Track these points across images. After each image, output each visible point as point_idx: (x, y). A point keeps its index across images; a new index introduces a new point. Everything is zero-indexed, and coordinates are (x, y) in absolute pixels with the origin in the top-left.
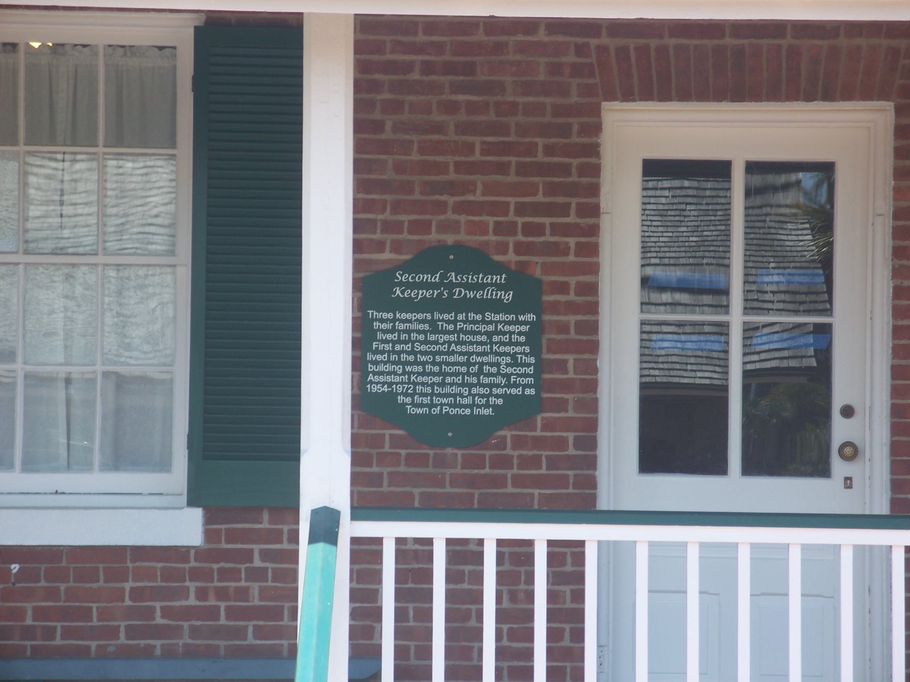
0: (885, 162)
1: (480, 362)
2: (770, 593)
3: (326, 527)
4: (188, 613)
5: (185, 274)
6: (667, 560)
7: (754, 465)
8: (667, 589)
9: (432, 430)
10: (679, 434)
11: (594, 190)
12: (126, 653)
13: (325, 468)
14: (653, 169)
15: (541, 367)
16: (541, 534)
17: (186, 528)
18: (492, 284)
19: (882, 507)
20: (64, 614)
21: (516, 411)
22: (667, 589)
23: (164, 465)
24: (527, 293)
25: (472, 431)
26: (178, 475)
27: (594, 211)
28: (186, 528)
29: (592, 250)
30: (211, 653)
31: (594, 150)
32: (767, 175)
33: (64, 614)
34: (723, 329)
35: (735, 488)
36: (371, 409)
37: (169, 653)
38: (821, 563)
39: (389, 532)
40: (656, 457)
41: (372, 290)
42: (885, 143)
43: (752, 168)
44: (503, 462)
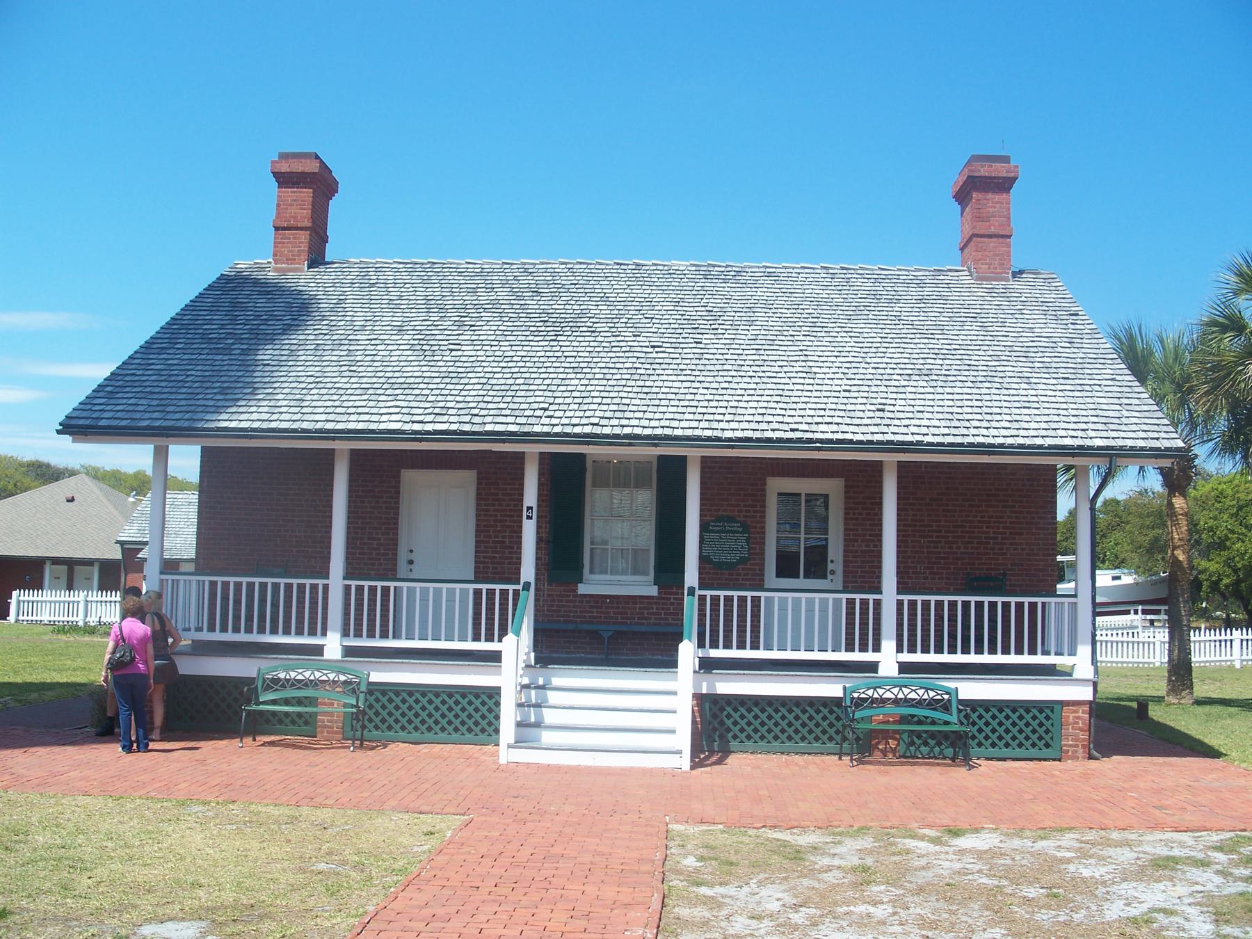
0: (842, 495)
1: (733, 547)
2: (810, 610)
3: (692, 592)
4: (654, 614)
5: (654, 522)
6: (783, 602)
7: (807, 576)
8: (783, 608)
9: (719, 566)
10: (787, 567)
11: (764, 501)
12: (637, 624)
13: (691, 576)
14: (779, 494)
15: (749, 549)
16: (749, 594)
17: (653, 591)
18: (736, 526)
19: (841, 588)
20: (621, 613)
21: (742, 561)
22: (783, 608)
23: (646, 573)
24: (746, 529)
25: (730, 566)
26: (651, 577)
27: (764, 507)
28: (653, 591)
29: (764, 517)
30: (659, 624)
31: (764, 490)
32: (811, 498)
33: (621, 613)
34: (799, 539)
35: (801, 582)
36: (703, 559)
37: (649, 624)
38: (824, 603)
39: (709, 593)
40: (781, 573)
41: (704, 527)
42: (842, 490)
43: (807, 495)
44: (739, 575)
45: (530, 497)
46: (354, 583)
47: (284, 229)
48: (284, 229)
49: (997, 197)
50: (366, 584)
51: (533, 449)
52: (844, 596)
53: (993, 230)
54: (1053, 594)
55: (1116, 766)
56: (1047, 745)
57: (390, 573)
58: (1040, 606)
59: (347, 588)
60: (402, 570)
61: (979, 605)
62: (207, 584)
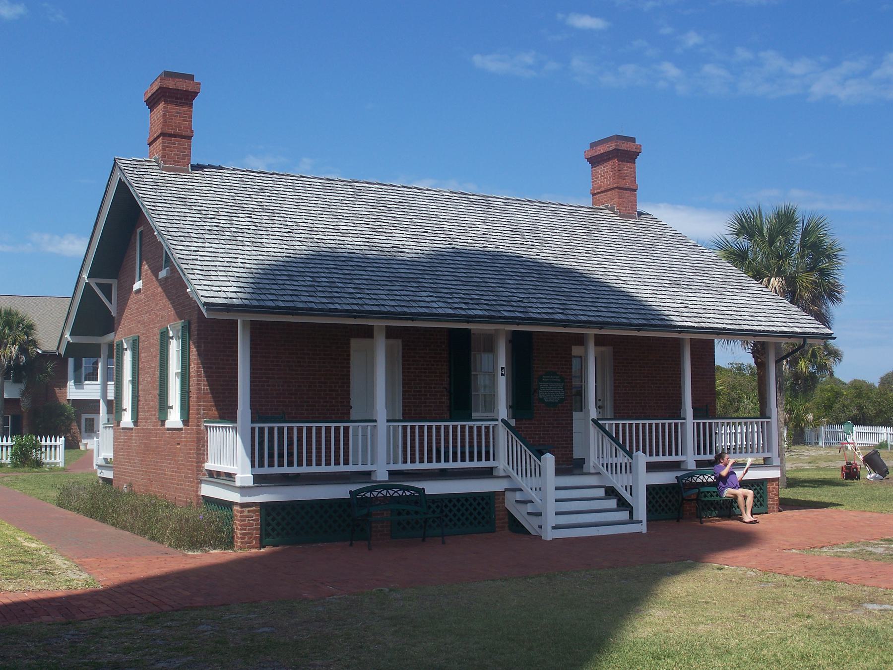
45: (502, 362)
46: (257, 425)
47: (171, 136)
48: (171, 136)
49: (629, 165)
50: (333, 425)
51: (688, 336)
52: (614, 422)
53: (628, 185)
54: (470, 419)
55: (788, 513)
56: (761, 505)
57: (345, 416)
58: (621, 426)
59: (253, 429)
60: (354, 415)
61: (637, 425)
62: (409, 428)
